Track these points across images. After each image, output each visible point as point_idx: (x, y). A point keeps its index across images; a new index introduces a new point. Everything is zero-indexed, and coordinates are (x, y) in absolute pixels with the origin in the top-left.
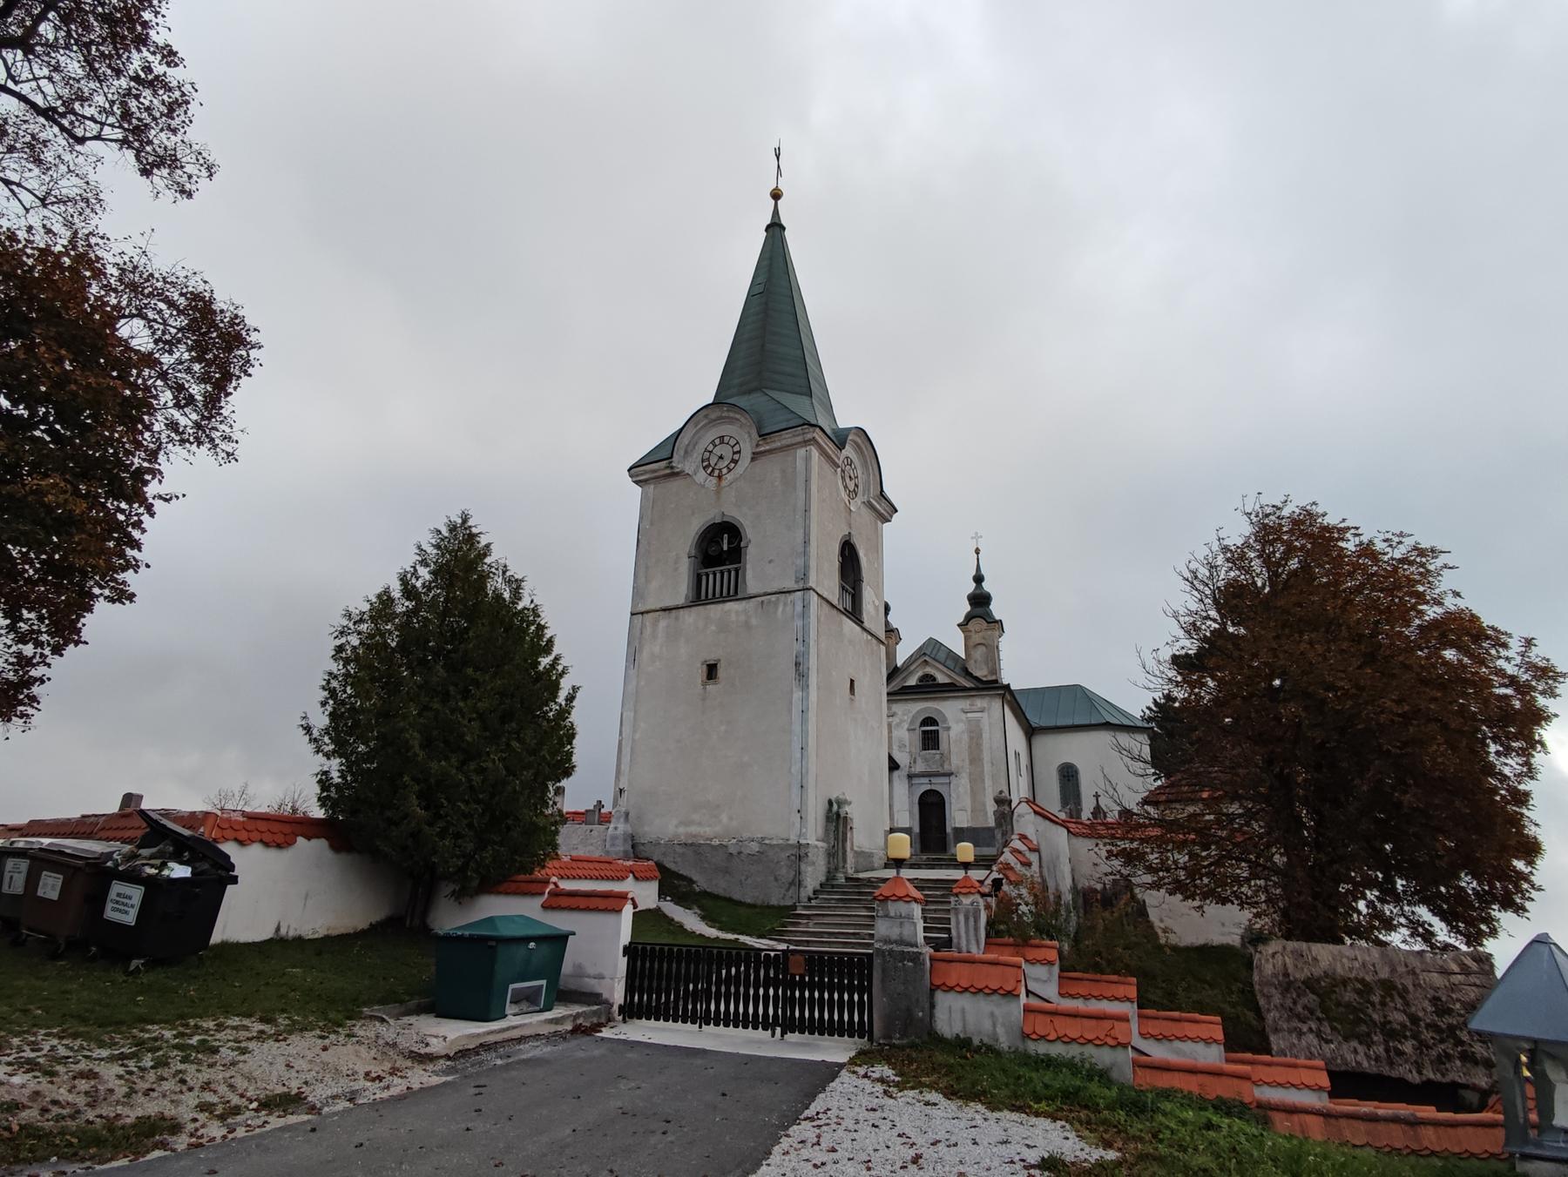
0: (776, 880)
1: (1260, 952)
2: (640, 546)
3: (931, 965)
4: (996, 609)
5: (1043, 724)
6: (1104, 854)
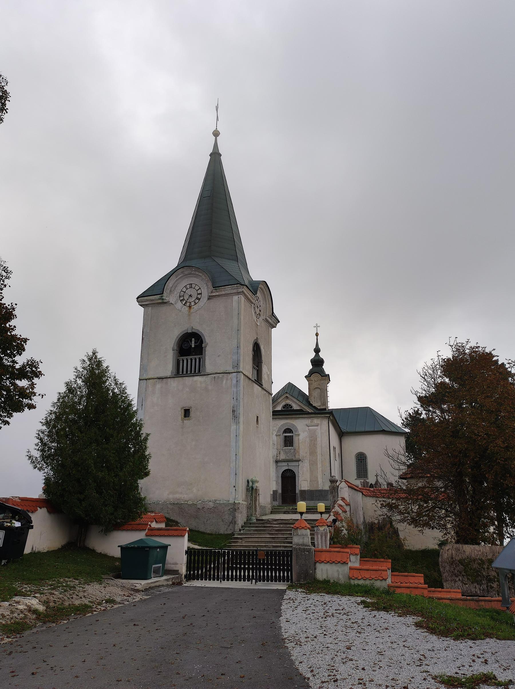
0: (223, 521)
1: (443, 549)
2: (144, 342)
3: (315, 553)
4: (327, 368)
5: (348, 430)
6: (379, 505)
